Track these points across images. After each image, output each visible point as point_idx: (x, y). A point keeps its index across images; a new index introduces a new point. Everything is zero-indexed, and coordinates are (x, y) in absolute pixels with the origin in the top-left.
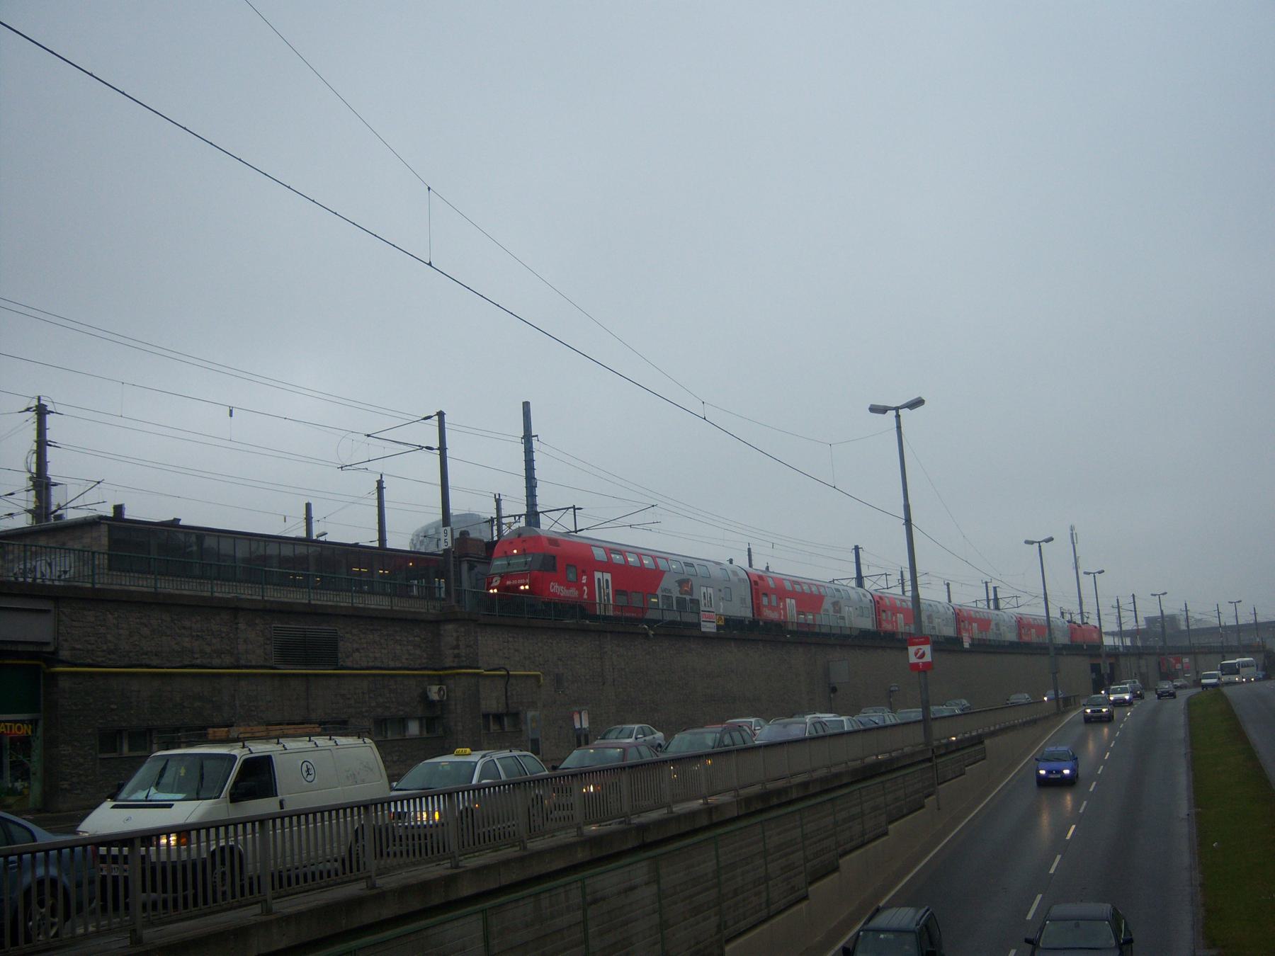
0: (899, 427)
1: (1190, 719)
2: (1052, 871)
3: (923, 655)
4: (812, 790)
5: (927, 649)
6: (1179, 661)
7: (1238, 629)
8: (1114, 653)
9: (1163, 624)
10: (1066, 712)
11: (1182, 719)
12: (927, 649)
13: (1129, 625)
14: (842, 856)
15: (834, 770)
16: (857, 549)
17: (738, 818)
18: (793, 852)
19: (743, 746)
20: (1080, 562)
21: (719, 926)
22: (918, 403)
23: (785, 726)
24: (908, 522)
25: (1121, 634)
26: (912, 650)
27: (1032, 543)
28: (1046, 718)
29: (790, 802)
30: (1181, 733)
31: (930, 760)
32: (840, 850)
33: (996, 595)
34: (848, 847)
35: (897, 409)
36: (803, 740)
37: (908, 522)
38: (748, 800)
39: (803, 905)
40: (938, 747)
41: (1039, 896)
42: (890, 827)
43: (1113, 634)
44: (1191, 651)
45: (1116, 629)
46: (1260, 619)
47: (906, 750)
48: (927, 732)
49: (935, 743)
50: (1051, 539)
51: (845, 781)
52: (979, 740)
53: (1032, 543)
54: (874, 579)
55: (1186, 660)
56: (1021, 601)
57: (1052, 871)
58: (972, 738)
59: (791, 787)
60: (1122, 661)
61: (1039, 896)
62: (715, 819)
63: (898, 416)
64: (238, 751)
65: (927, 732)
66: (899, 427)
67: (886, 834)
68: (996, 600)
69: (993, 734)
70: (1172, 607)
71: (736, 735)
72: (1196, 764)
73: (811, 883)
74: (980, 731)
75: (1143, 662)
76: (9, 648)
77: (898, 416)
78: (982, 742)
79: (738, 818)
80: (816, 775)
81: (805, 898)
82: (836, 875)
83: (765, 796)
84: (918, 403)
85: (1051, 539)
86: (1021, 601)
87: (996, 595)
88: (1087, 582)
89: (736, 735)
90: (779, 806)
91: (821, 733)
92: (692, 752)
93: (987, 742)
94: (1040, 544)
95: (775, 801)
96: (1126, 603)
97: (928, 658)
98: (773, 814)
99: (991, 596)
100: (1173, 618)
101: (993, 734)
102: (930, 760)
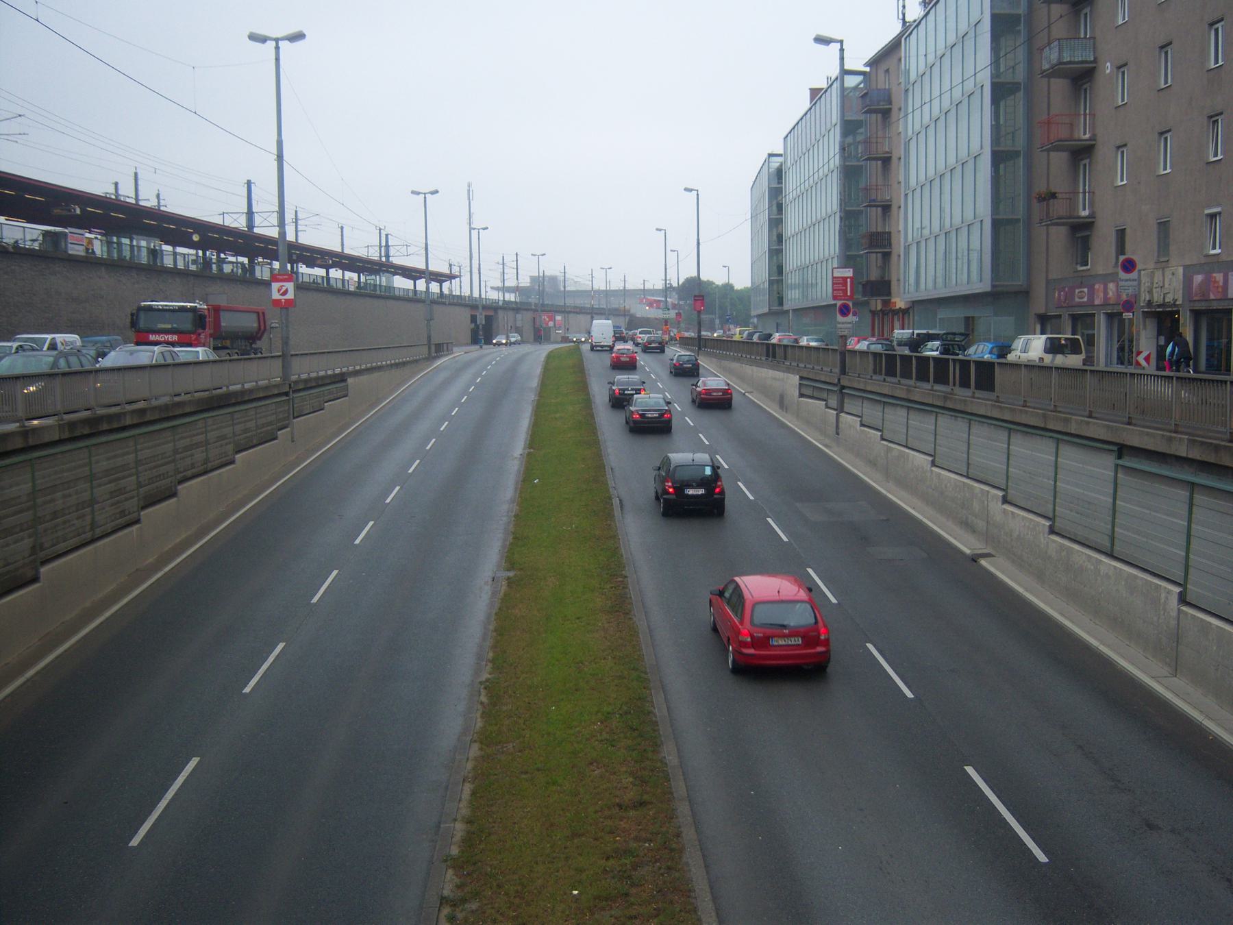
0: (277, 60)
1: (546, 369)
2: (388, 501)
3: (285, 293)
4: (149, 417)
5: (290, 286)
6: (552, 319)
7: (607, 294)
8: (493, 308)
9: (540, 282)
10: (438, 357)
11: (538, 370)
12: (290, 286)
13: (511, 282)
14: (180, 482)
15: (177, 399)
16: (249, 183)
17: (60, 442)
18: (124, 478)
19: (80, 369)
20: (474, 218)
21: (33, 548)
22: (299, 36)
23: (132, 353)
24: (280, 158)
25: (504, 289)
26: (275, 286)
27: (418, 193)
28: (416, 361)
29: (124, 428)
30: (535, 383)
31: (286, 394)
32: (179, 476)
33: (387, 242)
34: (189, 473)
35: (277, 40)
36: (152, 367)
37: (280, 158)
38: (72, 425)
39: (135, 528)
40: (296, 382)
41: (371, 523)
42: (237, 456)
43: (497, 289)
44: (564, 310)
45: (500, 285)
46: (629, 287)
47: (260, 383)
48: (286, 368)
49: (294, 378)
50: (437, 192)
51: (188, 410)
52: (342, 378)
53: (418, 193)
54: (265, 215)
55: (558, 318)
56: (410, 250)
57: (388, 501)
58: (335, 376)
59: (124, 414)
60: (501, 313)
61: (371, 523)
62: (31, 442)
63: (277, 48)
64: (50, 337)
65: (286, 368)
66: (277, 60)
67: (232, 462)
68: (387, 246)
69: (356, 373)
70: (551, 268)
71: (73, 360)
72: (540, 410)
73: (143, 508)
74: (344, 370)
75: (519, 316)
76: (1224, 331)
77: (277, 48)
78: (345, 381)
79: (60, 442)
80: (155, 403)
81: (137, 521)
82: (174, 500)
83: (94, 421)
84: (299, 36)
85: (437, 192)
86: (410, 250)
87: (387, 242)
88: (672, 257)
89: (73, 360)
90: (111, 431)
91: (170, 361)
92: (10, 373)
93: (350, 380)
94: (426, 196)
95: (105, 427)
96: (510, 260)
97: (290, 296)
98: (103, 439)
99: (383, 244)
100: (553, 279)
101: (356, 373)
102: (286, 394)
